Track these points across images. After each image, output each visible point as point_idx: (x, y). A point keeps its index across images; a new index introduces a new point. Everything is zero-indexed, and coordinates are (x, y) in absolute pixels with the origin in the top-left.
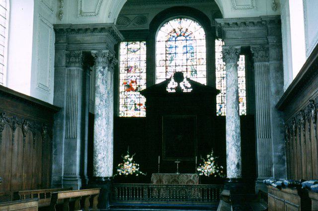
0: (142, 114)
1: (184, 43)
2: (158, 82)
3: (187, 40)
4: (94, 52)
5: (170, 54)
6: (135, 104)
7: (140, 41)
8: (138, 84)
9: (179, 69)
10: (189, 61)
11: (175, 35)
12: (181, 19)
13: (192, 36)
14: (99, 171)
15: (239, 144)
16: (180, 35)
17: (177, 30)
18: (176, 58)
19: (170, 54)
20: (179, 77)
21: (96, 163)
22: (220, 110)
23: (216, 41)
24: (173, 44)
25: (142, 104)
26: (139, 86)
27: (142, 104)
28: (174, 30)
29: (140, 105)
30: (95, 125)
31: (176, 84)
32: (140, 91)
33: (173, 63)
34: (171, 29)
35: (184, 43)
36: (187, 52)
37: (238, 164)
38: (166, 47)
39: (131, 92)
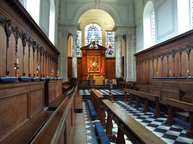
2: (86, 45)
3: (95, 31)
8: (78, 45)
9: (93, 41)
13: (97, 29)
16: (93, 29)
17: (92, 27)
20: (94, 43)
21: (74, 73)
29: (79, 53)
33: (91, 38)
34: (90, 27)
35: (94, 32)
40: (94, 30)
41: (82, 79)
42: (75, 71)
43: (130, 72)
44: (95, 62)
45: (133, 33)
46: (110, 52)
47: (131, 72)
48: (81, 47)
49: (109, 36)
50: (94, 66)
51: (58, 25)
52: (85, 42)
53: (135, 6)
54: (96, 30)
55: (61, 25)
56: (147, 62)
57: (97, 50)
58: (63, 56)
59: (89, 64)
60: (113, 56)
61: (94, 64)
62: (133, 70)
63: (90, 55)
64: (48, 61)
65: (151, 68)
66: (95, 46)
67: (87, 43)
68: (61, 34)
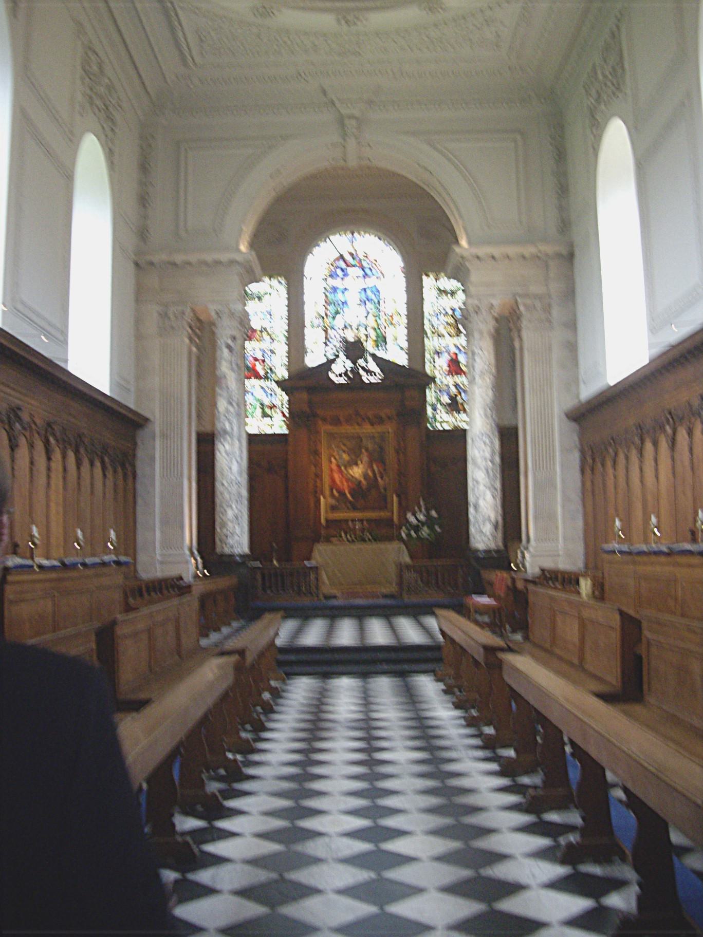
1: (362, 283)
4: (212, 308)
14: (230, 541)
15: (498, 485)
20: (354, 350)
21: (224, 525)
28: (342, 257)
29: (272, 407)
31: (349, 364)
33: (339, 322)
35: (362, 283)
37: (497, 522)
41: (36, 557)
42: (230, 514)
43: (546, 517)
44: (365, 459)
45: (555, 287)
46: (453, 399)
47: (552, 517)
49: (448, 303)
51: (137, 264)
55: (152, 264)
56: (621, 457)
58: (164, 436)
60: (460, 421)
61: (357, 472)
62: (566, 499)
63: (336, 422)
64: (65, 470)
66: (361, 362)
68: (153, 311)
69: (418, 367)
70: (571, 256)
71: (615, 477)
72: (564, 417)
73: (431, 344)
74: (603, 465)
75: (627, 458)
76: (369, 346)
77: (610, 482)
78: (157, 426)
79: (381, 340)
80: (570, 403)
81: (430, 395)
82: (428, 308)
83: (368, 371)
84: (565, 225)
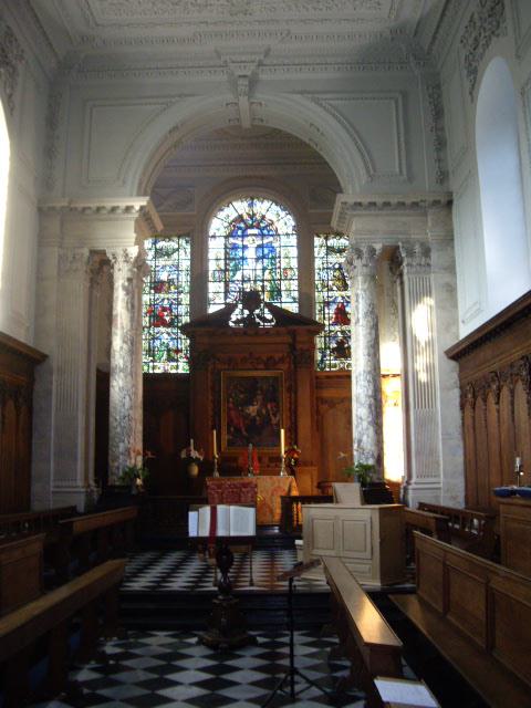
0: (182, 367)
2: (212, 309)
3: (263, 236)
5: (234, 259)
6: (169, 351)
7: (179, 237)
9: (248, 287)
10: (267, 272)
11: (242, 225)
12: (252, 199)
16: (252, 227)
17: (245, 217)
18: (245, 267)
19: (232, 259)
20: (251, 299)
22: (322, 360)
23: (316, 239)
24: (238, 242)
25: (181, 351)
26: (177, 317)
27: (181, 351)
29: (178, 351)
30: (111, 389)
32: (181, 328)
33: (238, 276)
34: (234, 215)
36: (263, 257)
38: (226, 247)
39: (162, 329)
40: (256, 231)
46: (340, 344)
48: (186, 319)
49: (335, 259)
50: (254, 420)
51: (40, 210)
52: (211, 296)
53: (439, 96)
54: (265, 232)
55: (54, 208)
56: (505, 392)
57: (267, 331)
59: (229, 409)
65: (523, 425)
66: (257, 311)
67: (220, 299)
68: (53, 254)
69: (305, 315)
70: (450, 203)
71: (498, 411)
72: (443, 355)
73: (320, 296)
74: (485, 400)
75: (512, 392)
76: (266, 297)
77: (493, 416)
78: (54, 362)
79: (277, 292)
80: (450, 343)
81: (319, 342)
82: (318, 263)
83: (265, 320)
84: (443, 177)
